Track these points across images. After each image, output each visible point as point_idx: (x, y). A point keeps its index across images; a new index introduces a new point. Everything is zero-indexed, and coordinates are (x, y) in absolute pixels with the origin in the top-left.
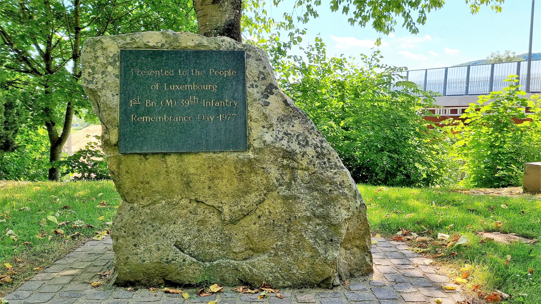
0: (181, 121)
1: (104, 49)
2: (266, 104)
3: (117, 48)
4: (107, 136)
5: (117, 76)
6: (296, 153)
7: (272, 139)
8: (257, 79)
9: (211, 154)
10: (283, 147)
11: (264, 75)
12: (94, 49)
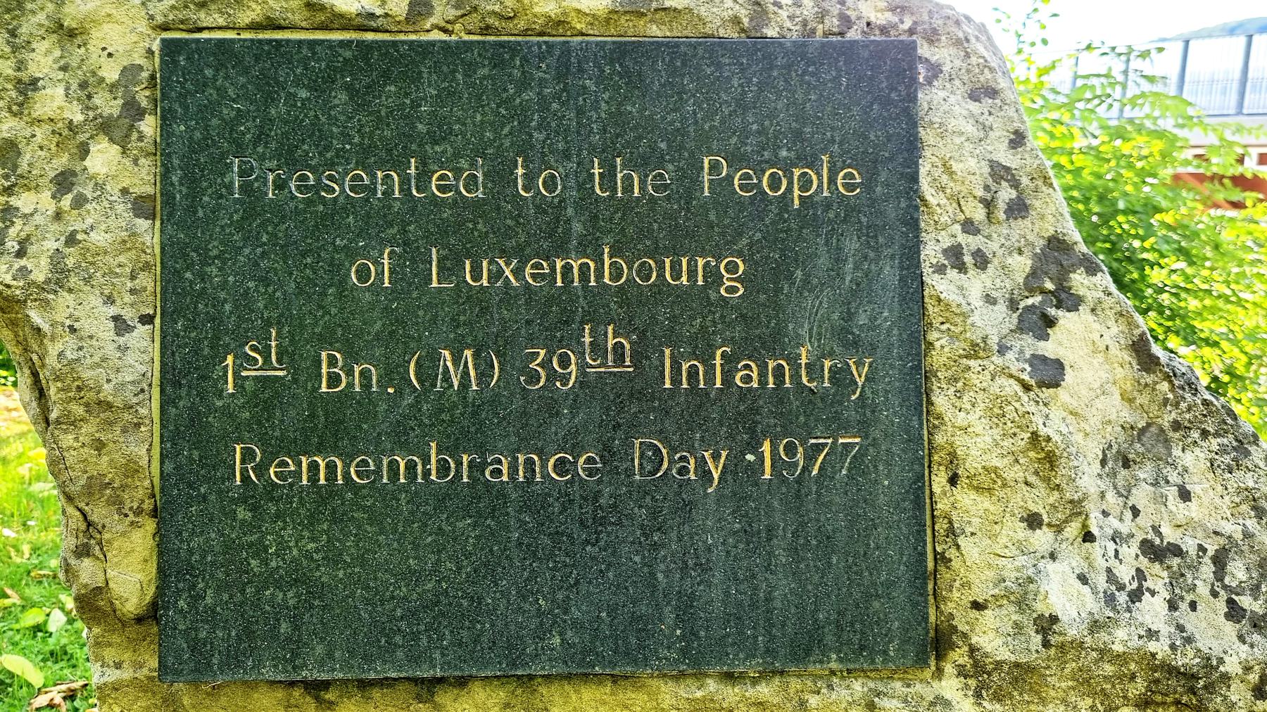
0: (530, 480)
1: (72, 34)
2: (1048, 374)
3: (143, 26)
4: (88, 571)
5: (142, 207)
6: (1226, 678)
7: (1092, 604)
8: (979, 214)
9: (712, 685)
10: (1152, 646)
11: (1015, 184)
12: (13, 33)
